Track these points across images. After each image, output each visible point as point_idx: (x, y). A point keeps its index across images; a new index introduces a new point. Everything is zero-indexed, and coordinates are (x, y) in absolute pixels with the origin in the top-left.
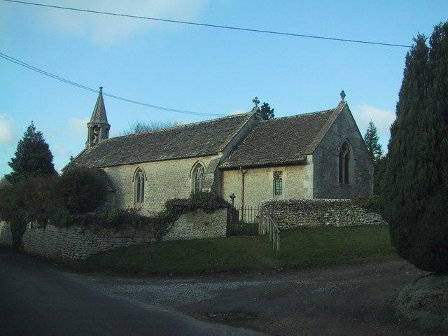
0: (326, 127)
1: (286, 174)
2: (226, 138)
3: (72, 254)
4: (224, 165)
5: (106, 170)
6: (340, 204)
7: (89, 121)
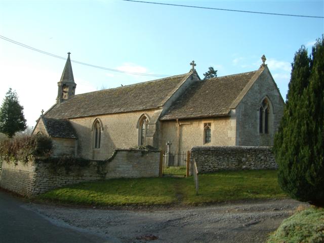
0: (246, 89)
1: (214, 126)
2: (167, 95)
3: (33, 189)
4: (164, 118)
5: (71, 120)
6: (255, 150)
7: (59, 81)
